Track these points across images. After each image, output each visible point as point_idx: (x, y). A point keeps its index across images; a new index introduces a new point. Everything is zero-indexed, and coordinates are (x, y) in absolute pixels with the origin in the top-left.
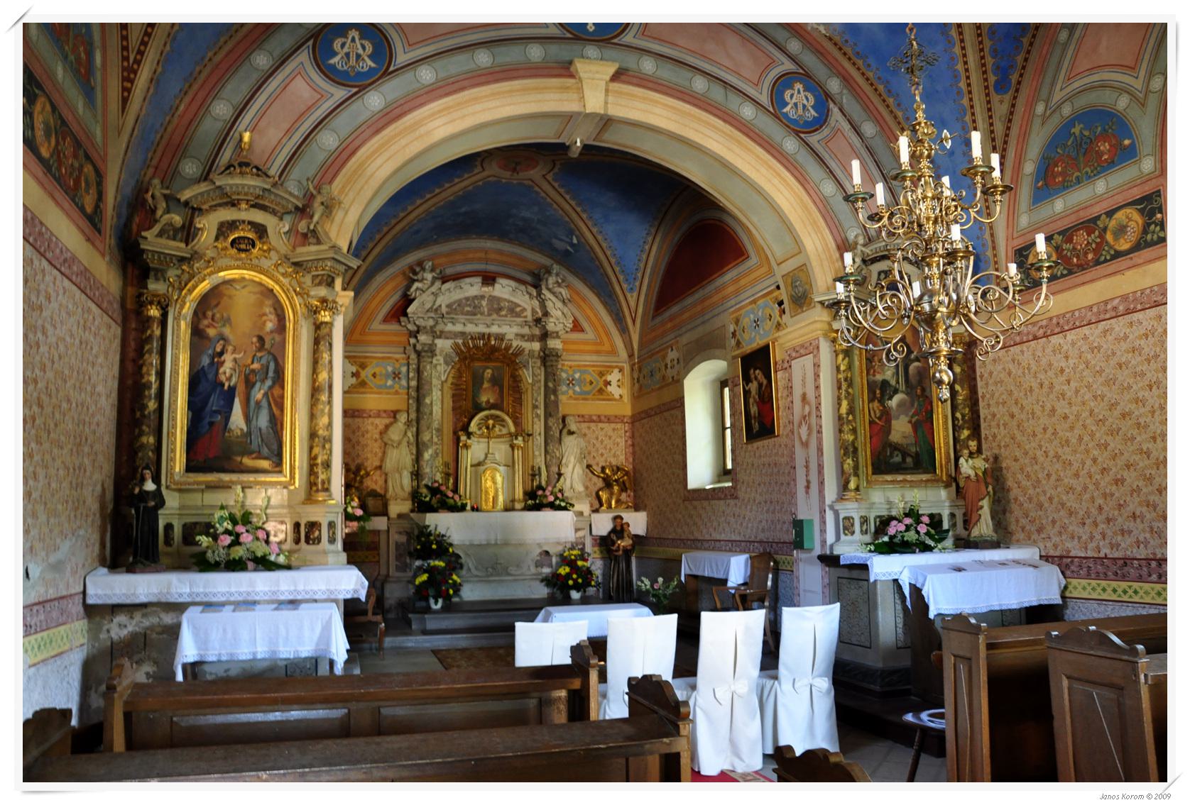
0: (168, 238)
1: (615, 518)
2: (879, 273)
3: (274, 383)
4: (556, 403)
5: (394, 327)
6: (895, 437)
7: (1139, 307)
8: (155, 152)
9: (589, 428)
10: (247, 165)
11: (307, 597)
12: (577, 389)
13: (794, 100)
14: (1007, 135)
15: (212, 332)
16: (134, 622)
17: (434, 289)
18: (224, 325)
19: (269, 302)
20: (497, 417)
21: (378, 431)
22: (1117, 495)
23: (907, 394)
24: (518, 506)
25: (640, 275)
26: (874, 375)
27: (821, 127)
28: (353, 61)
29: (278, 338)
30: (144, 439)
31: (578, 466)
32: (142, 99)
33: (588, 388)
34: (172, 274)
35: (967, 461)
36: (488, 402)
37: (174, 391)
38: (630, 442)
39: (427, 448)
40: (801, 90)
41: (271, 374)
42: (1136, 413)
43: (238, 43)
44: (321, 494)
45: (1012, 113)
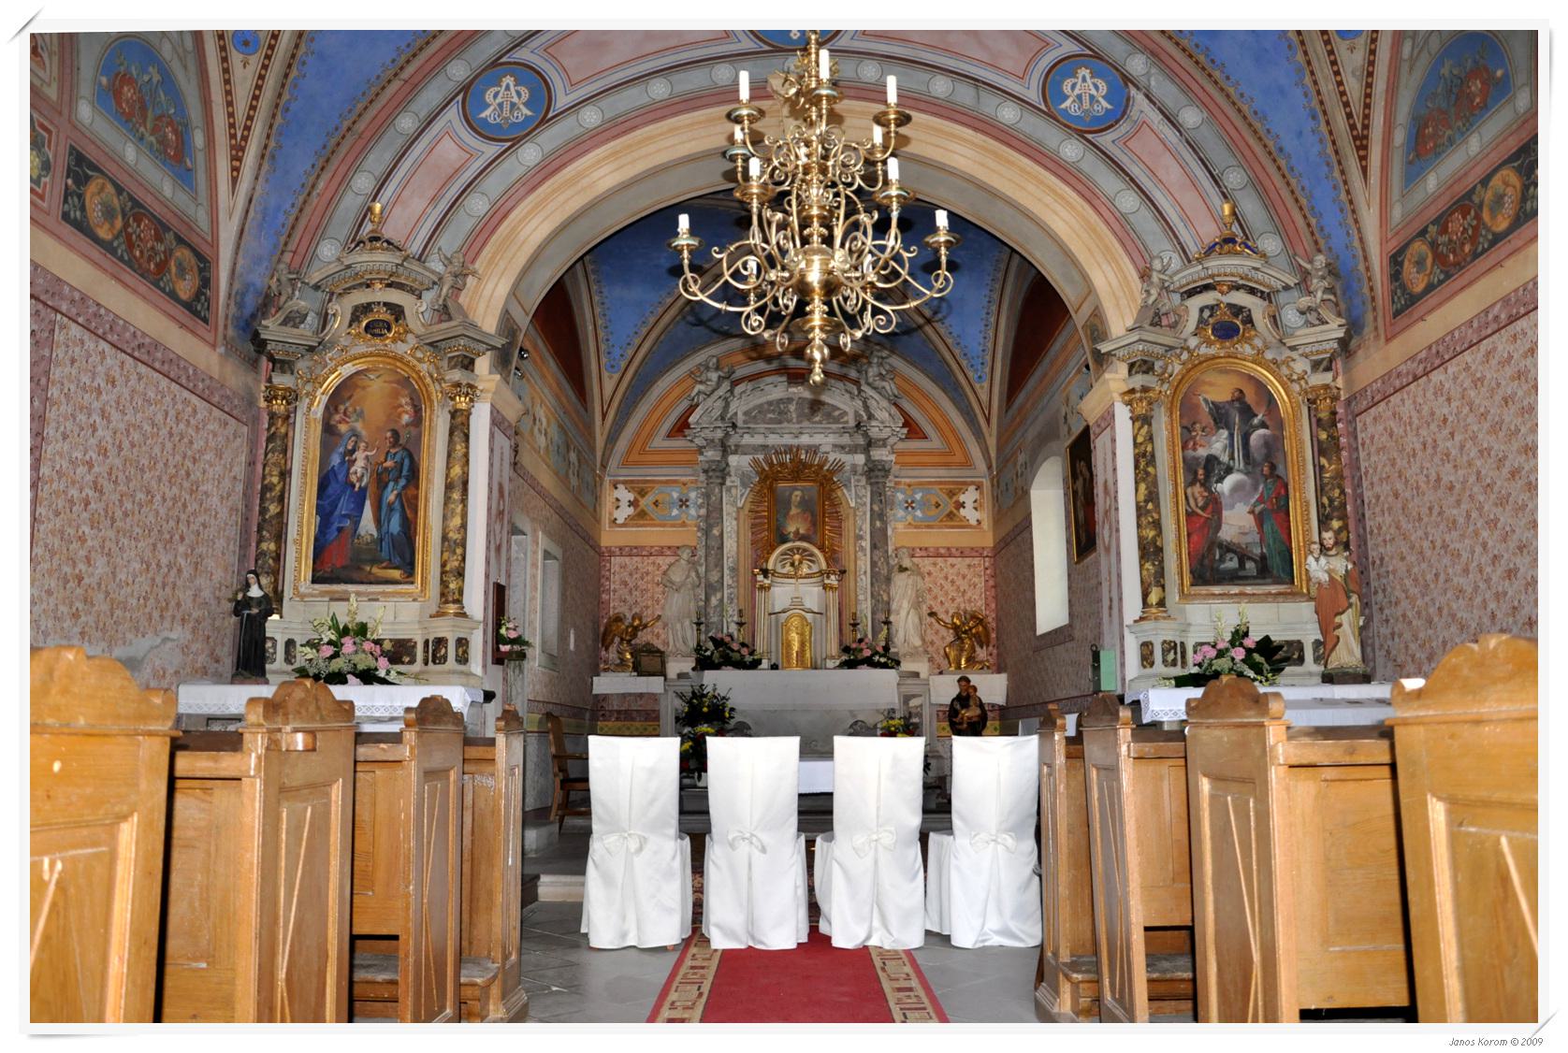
2: (1202, 310)
3: (408, 481)
4: (884, 531)
5: (678, 443)
6: (1227, 533)
7: (1522, 310)
9: (935, 564)
10: (377, 239)
12: (919, 513)
13: (1077, 91)
14: (1368, 96)
15: (343, 428)
17: (721, 392)
20: (805, 550)
22: (1510, 594)
23: (1247, 474)
24: (830, 664)
25: (988, 358)
26: (1195, 449)
27: (1117, 122)
29: (413, 431)
34: (302, 366)
35: (1317, 560)
36: (797, 532)
38: (991, 583)
40: (1088, 77)
42: (1527, 468)
44: (451, 605)
45: (1372, 63)
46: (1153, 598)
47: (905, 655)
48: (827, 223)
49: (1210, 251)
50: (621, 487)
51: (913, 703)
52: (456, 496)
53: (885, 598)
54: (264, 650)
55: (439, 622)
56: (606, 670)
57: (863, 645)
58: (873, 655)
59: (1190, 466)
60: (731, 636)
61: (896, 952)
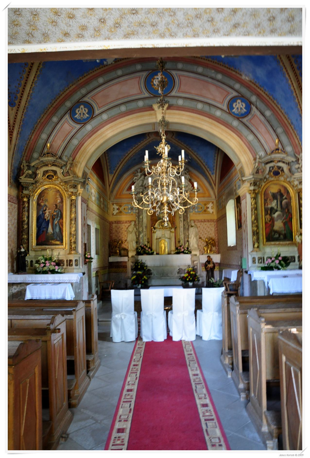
0: (28, 178)
1: (208, 257)
2: (270, 168)
8: (25, 152)
10: (49, 153)
11: (63, 282)
15: (42, 204)
16: (18, 288)
18: (46, 202)
19: (58, 194)
21: (126, 228)
23: (281, 211)
25: (215, 168)
26: (267, 205)
27: (248, 115)
28: (82, 116)
29: (61, 204)
30: (24, 237)
31: (195, 238)
32: (15, 139)
33: (200, 210)
34: (30, 188)
35: (298, 236)
37: (32, 222)
38: (216, 229)
39: (141, 233)
40: (240, 103)
41: (59, 216)
43: (48, 115)
44: (73, 251)
46: (256, 246)
47: (193, 250)
48: (168, 186)
49: (272, 152)
50: (115, 205)
51: (195, 263)
52: (73, 222)
53: (187, 234)
54: (25, 264)
55: (70, 256)
56: (113, 255)
57: (181, 248)
58: (184, 250)
59: (266, 210)
60: (145, 245)
61: (188, 342)
